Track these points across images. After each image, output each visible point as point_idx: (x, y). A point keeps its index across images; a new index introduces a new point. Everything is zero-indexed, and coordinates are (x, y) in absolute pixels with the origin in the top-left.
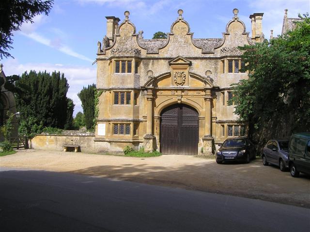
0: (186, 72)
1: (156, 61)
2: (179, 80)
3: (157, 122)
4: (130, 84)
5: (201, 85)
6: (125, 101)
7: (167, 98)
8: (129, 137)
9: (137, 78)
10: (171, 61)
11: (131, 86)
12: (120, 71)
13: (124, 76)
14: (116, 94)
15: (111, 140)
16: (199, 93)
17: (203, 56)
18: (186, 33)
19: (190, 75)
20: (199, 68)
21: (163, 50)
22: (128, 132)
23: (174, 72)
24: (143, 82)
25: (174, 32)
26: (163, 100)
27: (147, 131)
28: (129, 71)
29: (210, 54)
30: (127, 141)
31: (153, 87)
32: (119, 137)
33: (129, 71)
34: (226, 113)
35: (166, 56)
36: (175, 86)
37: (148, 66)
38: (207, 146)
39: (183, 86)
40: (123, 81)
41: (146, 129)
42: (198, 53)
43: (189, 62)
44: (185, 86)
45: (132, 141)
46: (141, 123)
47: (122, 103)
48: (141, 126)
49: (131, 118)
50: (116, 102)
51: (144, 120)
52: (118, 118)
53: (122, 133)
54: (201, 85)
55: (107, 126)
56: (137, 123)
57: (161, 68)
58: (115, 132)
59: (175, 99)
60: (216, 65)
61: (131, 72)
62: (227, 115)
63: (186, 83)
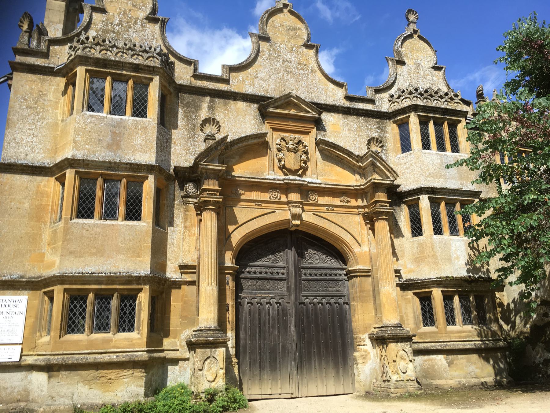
0: (309, 141)
1: (222, 101)
2: (291, 161)
3: (245, 179)
4: (144, 152)
5: (353, 180)
6: (121, 210)
7: (259, 212)
8: (133, 341)
9: (164, 145)
10: (264, 105)
11: (148, 157)
12: (97, 213)
13: (118, 125)
14: (76, 299)
15: (54, 360)
16: (348, 202)
17: (347, 104)
18: (302, 42)
19: (321, 151)
20: (344, 132)
21: (241, 75)
22: (126, 323)
23: (274, 138)
24: (182, 156)
25: (270, 31)
26: (251, 217)
27: (202, 316)
28: (133, 213)
29: (349, 236)
30: (123, 358)
31: (212, 180)
32: (85, 342)
33: (133, 213)
34: (434, 256)
35: (249, 90)
36: (278, 176)
37: (197, 111)
38: (402, 358)
39: (303, 179)
40: (116, 138)
41: (200, 307)
42: (336, 96)
43: (314, 115)
44: (309, 179)
45: (144, 356)
46: (175, 293)
47: (110, 213)
48: (177, 300)
49: (142, 267)
50: (84, 210)
51: (188, 278)
52: (88, 269)
53: (102, 327)
54: (353, 180)
55: (36, 302)
56: (162, 289)
57: (239, 122)
58: (71, 324)
59: (282, 215)
60: (382, 131)
61: (131, 329)
62: (436, 263)
63: (309, 172)
